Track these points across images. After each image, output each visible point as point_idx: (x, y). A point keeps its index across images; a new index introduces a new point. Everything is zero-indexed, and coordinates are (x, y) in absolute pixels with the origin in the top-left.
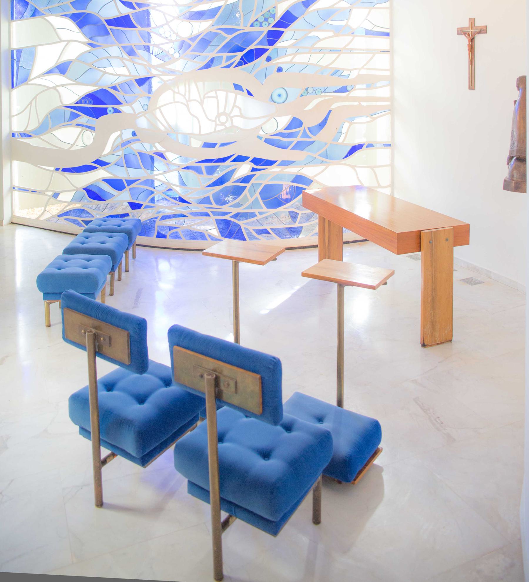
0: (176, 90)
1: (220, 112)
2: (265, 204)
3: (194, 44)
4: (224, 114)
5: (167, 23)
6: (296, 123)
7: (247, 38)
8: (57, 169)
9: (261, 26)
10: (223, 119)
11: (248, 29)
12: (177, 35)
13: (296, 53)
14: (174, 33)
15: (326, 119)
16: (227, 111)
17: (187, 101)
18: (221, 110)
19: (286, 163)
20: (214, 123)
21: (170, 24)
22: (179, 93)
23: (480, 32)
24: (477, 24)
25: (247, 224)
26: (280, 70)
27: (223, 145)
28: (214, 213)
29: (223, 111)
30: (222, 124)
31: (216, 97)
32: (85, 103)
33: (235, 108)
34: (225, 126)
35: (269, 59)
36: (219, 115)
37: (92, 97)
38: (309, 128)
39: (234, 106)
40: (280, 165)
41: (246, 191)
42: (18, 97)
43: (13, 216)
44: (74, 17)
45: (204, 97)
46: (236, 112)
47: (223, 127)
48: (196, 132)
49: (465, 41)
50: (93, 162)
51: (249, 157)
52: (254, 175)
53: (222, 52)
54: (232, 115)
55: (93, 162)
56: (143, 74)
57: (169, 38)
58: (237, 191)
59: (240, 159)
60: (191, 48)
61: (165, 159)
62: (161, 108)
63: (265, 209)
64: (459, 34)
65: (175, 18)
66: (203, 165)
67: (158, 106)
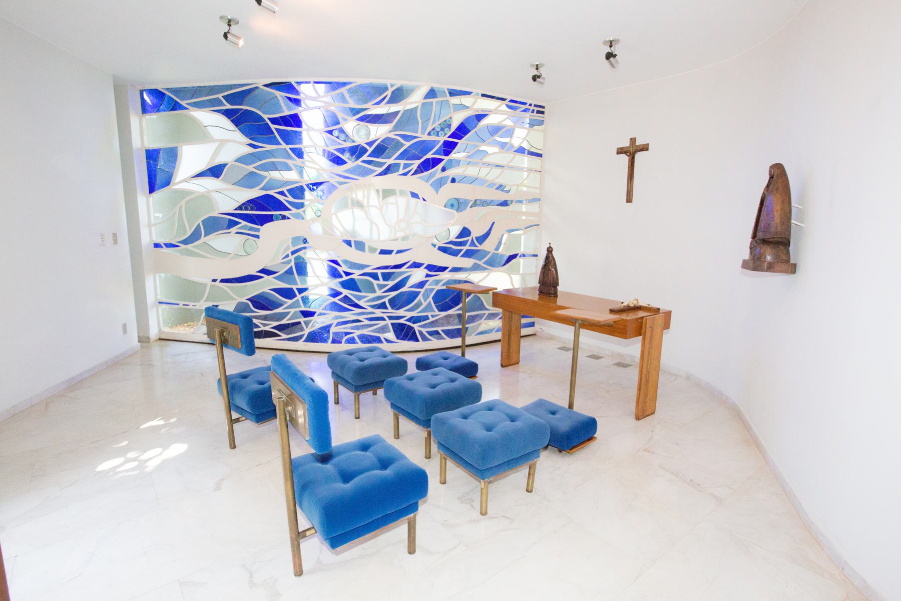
2: (437, 307)
3: (370, 150)
6: (465, 232)
7: (425, 147)
8: (214, 281)
9: (438, 135)
11: (425, 137)
15: (490, 230)
19: (456, 270)
23: (642, 150)
24: (638, 143)
25: (420, 326)
27: (399, 252)
28: (390, 318)
32: (246, 209)
35: (444, 169)
37: (254, 203)
40: (451, 271)
41: (420, 297)
43: (160, 331)
44: (228, 113)
48: (375, 237)
49: (625, 159)
52: (427, 281)
58: (413, 296)
59: (416, 265)
63: (437, 312)
64: (618, 153)
66: (379, 272)
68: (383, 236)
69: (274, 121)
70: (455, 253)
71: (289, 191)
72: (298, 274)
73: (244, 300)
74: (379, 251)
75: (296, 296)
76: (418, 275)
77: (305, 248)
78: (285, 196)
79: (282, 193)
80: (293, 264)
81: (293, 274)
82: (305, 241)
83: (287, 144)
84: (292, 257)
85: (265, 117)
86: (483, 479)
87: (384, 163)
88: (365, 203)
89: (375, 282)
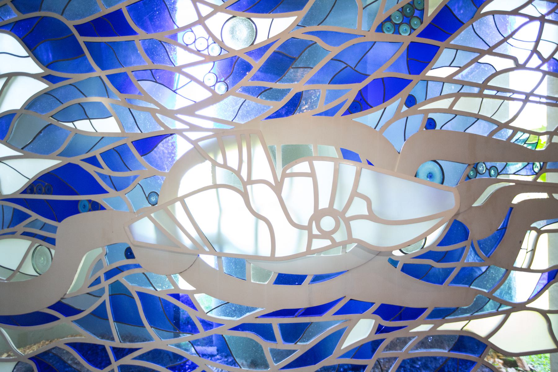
0: (220, 160)
1: (321, 207)
3: (257, 64)
4: (330, 211)
5: (201, 21)
6: (457, 232)
10: (328, 223)
12: (222, 47)
13: (457, 96)
14: (215, 41)
16: (336, 207)
17: (245, 184)
18: (324, 204)
19: (441, 314)
20: (306, 232)
21: (208, 22)
22: (225, 166)
26: (431, 124)
29: (327, 206)
30: (325, 235)
31: (312, 174)
32: (40, 192)
33: (356, 200)
34: (333, 240)
36: (318, 215)
39: (355, 193)
42: (543, 262)
45: (284, 175)
46: (359, 207)
48: (265, 251)
50: (49, 308)
51: (373, 304)
54: (349, 214)
55: (49, 308)
56: (149, 129)
57: (205, 52)
59: (354, 307)
60: (254, 71)
61: (196, 309)
62: (186, 200)
65: (216, 9)
66: (276, 323)
67: (180, 194)
69: (83, 30)
70: (438, 279)
72: (117, 319)
73: (386, 33)
75: (110, 363)
76: (362, 329)
78: (100, 166)
79: (93, 161)
80: (106, 297)
82: (129, 254)
84: (105, 284)
85: (70, 24)
87: (284, 92)
89: (267, 346)
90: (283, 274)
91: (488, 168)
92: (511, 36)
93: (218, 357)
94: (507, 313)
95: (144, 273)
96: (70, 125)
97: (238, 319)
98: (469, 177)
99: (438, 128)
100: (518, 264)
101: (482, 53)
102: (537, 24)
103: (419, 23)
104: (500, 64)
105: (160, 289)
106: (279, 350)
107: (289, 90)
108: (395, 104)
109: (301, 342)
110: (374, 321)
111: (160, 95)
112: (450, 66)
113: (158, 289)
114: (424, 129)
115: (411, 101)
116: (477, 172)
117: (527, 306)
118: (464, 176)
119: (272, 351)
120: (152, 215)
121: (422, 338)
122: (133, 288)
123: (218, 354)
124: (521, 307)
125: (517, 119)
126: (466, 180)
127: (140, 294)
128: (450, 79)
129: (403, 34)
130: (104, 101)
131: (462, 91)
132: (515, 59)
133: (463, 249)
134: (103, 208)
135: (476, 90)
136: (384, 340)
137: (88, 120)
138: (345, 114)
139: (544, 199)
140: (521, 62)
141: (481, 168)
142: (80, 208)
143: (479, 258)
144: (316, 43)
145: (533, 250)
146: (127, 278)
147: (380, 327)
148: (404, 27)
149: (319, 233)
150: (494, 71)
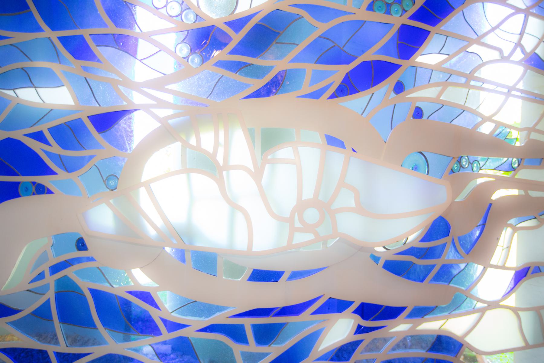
3: (237, 38)
4: (315, 203)
6: (439, 228)
9: (388, 12)
13: (446, 84)
18: (308, 194)
19: (421, 312)
26: (418, 113)
30: (307, 228)
38: (459, 238)
46: (347, 200)
47: (310, 237)
48: (241, 244)
53: (303, 61)
62: (153, 185)
66: (248, 323)
68: (262, 237)
71: (54, 131)
72: (63, 319)
74: (248, 273)
76: (340, 330)
77: (78, 260)
78: (46, 142)
79: (39, 136)
80: (51, 295)
81: (49, 318)
82: (81, 245)
83: (54, 28)
84: (50, 280)
86: (192, 51)
88: (220, 158)
89: (237, 349)
90: (258, 270)
91: (471, 162)
92: (498, 27)
93: (172, 356)
94: (483, 311)
95: (98, 268)
96: (10, 93)
97: (207, 319)
98: (452, 171)
99: (425, 117)
100: (493, 261)
101: (471, 42)
102: (522, 16)
103: (411, 4)
104: (486, 54)
105: (118, 286)
106: (251, 353)
107: (272, 67)
108: (384, 89)
109: (276, 344)
110: (353, 321)
111: (124, 64)
112: (439, 53)
113: (114, 286)
114: (412, 118)
115: (399, 88)
116: (461, 166)
117: (501, 303)
118: (448, 170)
119: (243, 354)
120: (111, 201)
121: (401, 338)
122: (85, 285)
123: (172, 353)
124: (493, 305)
125: (501, 112)
126: (450, 174)
127: (94, 292)
128: (439, 68)
129: (394, 15)
130: (55, 67)
131: (450, 80)
132: (500, 51)
133: (444, 245)
134: (50, 192)
135: (463, 80)
136: (362, 341)
137: (34, 89)
138: (333, 96)
139: (515, 196)
140: (506, 54)
141: (464, 162)
142: (20, 191)
143: (458, 255)
144: (303, 17)
145: (509, 247)
146: (77, 273)
147: (359, 327)
148: (395, 8)
149: (301, 226)
150: (481, 62)
